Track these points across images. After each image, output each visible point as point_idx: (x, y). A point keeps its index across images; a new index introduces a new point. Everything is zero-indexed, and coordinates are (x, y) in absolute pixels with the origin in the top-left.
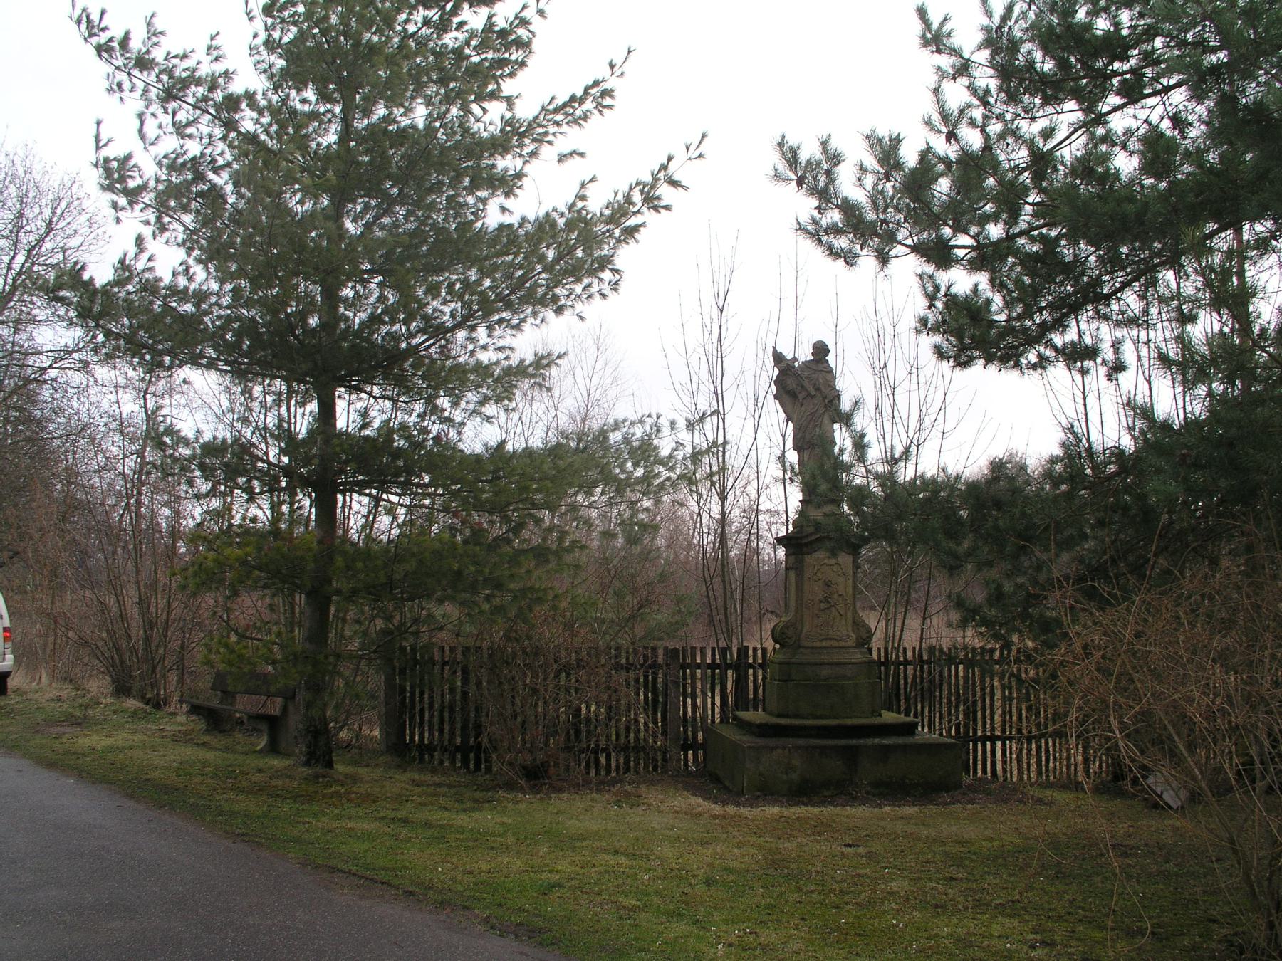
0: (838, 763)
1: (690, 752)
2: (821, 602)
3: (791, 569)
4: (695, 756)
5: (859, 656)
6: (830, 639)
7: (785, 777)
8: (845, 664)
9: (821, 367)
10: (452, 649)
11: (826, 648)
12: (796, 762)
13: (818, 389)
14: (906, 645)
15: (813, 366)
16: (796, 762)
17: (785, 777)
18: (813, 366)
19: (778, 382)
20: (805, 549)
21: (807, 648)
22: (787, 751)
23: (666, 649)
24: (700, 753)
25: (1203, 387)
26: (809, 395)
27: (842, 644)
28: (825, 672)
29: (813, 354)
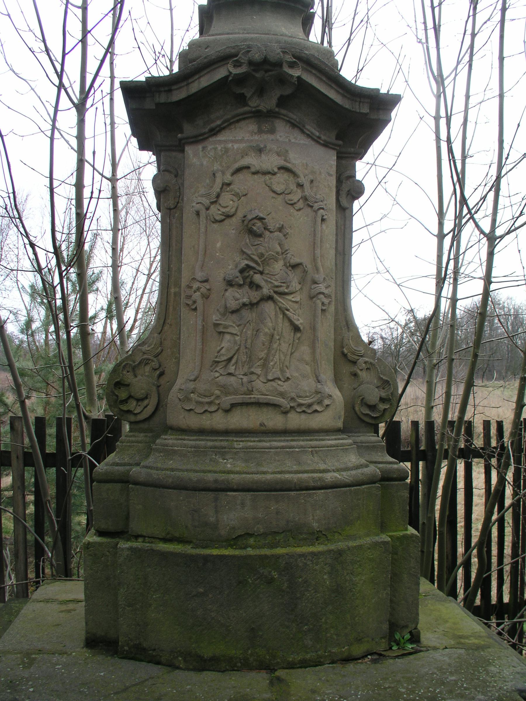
2: (230, 283)
5: (353, 459)
6: (258, 404)
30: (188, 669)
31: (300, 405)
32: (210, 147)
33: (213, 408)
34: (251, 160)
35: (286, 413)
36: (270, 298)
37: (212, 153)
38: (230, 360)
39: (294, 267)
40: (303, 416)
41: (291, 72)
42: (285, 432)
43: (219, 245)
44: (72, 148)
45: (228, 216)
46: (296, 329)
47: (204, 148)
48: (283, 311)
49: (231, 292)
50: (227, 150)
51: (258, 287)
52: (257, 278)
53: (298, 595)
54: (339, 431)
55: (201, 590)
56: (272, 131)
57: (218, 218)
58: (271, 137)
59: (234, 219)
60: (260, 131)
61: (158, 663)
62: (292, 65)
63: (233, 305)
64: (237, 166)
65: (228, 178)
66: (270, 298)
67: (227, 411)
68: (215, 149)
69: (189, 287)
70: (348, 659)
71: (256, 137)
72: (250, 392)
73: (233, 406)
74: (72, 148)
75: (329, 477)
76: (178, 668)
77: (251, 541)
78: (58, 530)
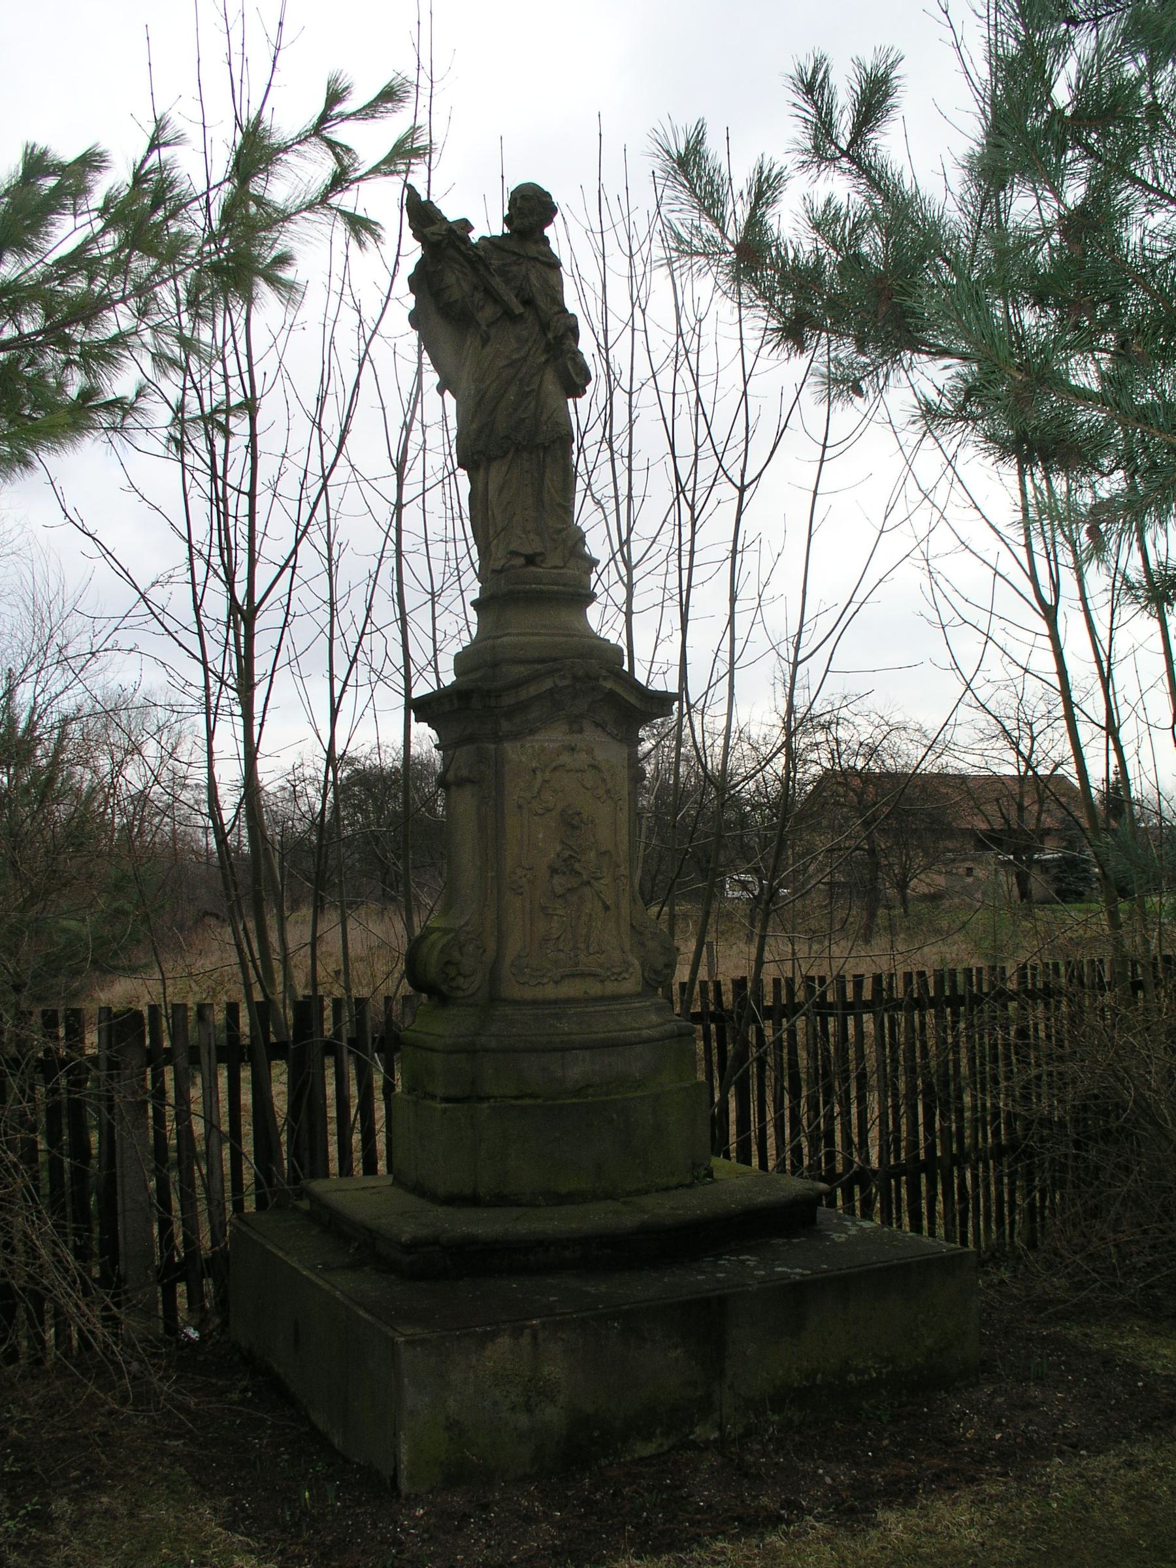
0: (673, 1354)
1: (181, 1288)
2: (554, 871)
3: (461, 783)
4: (195, 1297)
5: (654, 1018)
6: (583, 975)
7: (523, 1420)
8: (630, 1044)
9: (532, 250)
10: (858, 981)
11: (568, 1001)
12: (555, 1369)
13: (528, 302)
14: (720, 978)
15: (513, 246)
16: (555, 1369)
17: (523, 1420)
18: (513, 246)
19: (420, 281)
20: (505, 725)
21: (516, 1003)
22: (526, 1340)
23: (727, 1156)
24: (208, 1285)
25: (334, 914)
26: (509, 316)
27: (611, 988)
28: (578, 1069)
29: (507, 220)
30: (547, 1205)
31: (613, 974)
32: (528, 745)
33: (545, 980)
34: (565, 758)
35: (602, 981)
36: (588, 883)
37: (530, 751)
38: (558, 938)
39: (605, 853)
40: (616, 984)
41: (604, 684)
42: (601, 999)
43: (540, 836)
44: (195, 657)
45: (549, 810)
46: (607, 908)
47: (522, 746)
48: (598, 894)
49: (557, 880)
50: (543, 750)
51: (579, 874)
52: (577, 866)
53: (944, 924)
54: (639, 995)
55: (558, 1135)
56: (581, 731)
57: (540, 811)
58: (580, 736)
59: (554, 813)
60: (571, 732)
61: (520, 1205)
62: (605, 678)
63: (559, 890)
64: (554, 764)
65: (547, 776)
66: (588, 883)
67: (556, 983)
68: (533, 747)
69: (514, 873)
70: (667, 1189)
71: (569, 737)
72: (577, 964)
73: (563, 977)
74: (195, 657)
75: (646, 1033)
76: (539, 1206)
77: (591, 1091)
78: (90, 1195)
